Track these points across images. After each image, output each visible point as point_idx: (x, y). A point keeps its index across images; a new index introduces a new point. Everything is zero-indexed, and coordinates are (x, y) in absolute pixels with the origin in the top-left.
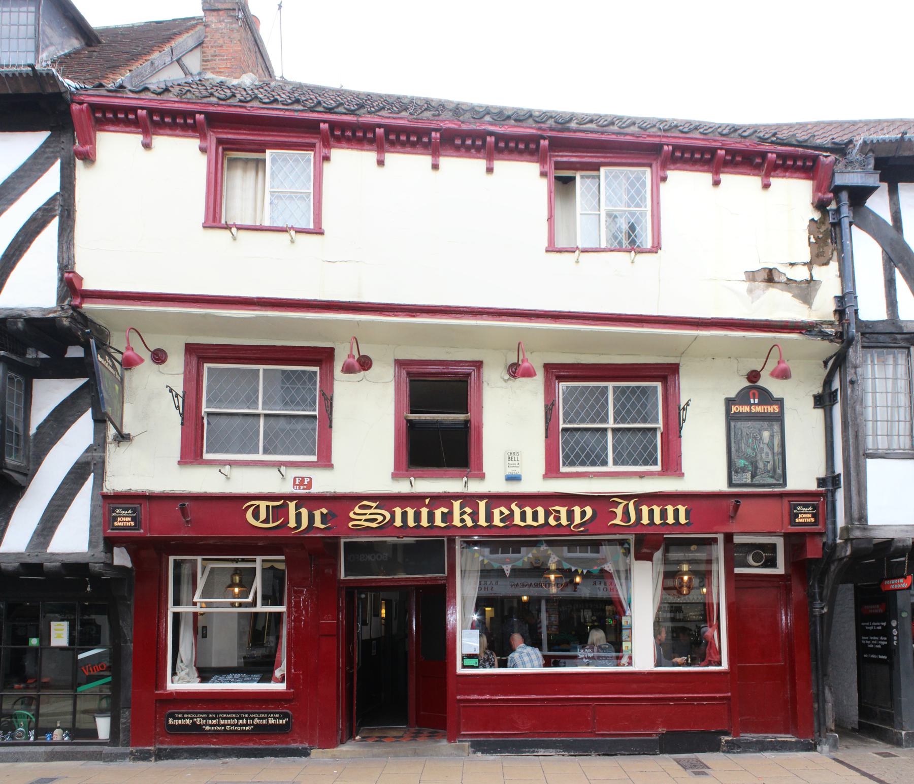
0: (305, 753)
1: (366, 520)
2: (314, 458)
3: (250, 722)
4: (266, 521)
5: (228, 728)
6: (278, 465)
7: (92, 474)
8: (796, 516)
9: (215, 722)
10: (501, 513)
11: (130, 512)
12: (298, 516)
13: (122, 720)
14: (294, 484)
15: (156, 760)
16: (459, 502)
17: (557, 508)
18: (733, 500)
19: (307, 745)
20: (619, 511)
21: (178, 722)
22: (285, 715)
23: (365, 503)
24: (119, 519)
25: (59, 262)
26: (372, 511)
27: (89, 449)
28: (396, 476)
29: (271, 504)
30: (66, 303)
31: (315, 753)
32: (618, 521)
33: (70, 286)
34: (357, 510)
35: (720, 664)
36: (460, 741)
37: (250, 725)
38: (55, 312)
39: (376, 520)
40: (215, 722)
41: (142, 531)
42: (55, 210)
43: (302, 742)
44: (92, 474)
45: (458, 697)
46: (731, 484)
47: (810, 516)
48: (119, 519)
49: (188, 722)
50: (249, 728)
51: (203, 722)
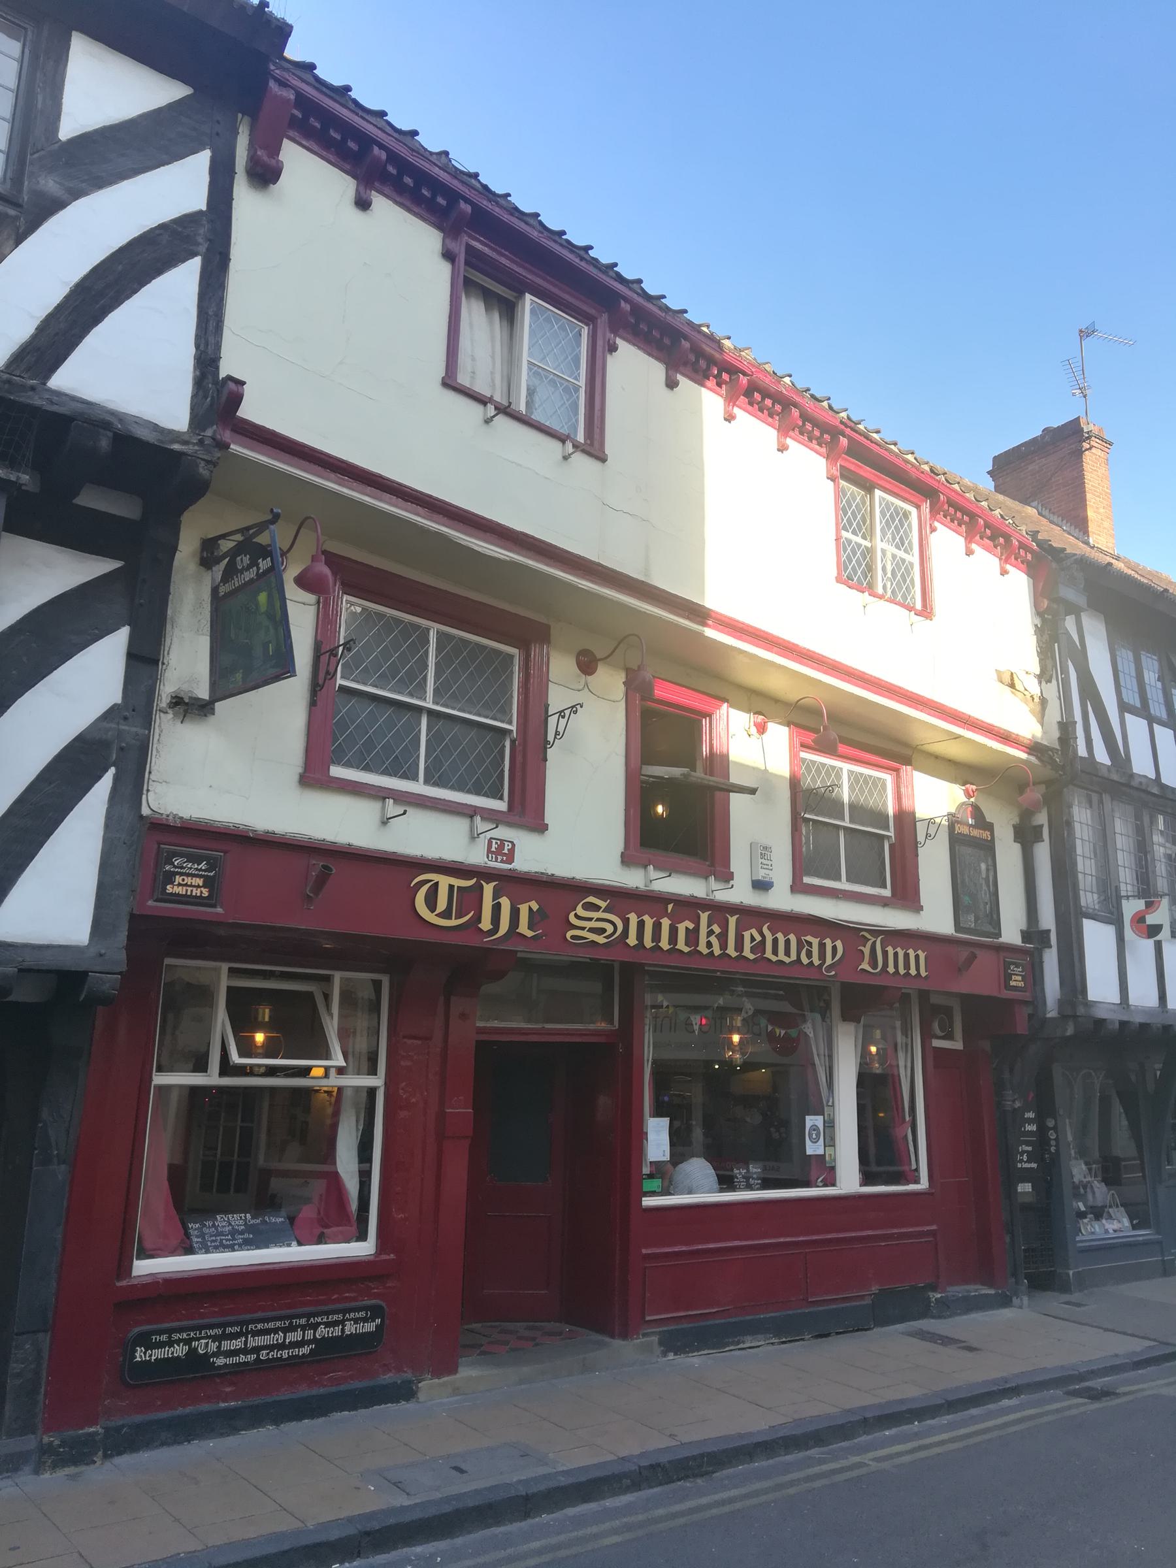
0: (406, 1392)
1: (591, 930)
2: (501, 806)
3: (309, 1334)
4: (446, 914)
5: (263, 1355)
6: (470, 813)
7: (112, 770)
8: (169, 878)
9: (238, 1344)
10: (753, 939)
11: (203, 866)
12: (497, 908)
13: (15, 1367)
14: (489, 851)
15: (106, 1456)
16: (707, 914)
17: (809, 938)
18: (318, 863)
19: (408, 1375)
20: (867, 950)
21: (157, 1354)
22: (376, 1312)
23: (591, 899)
24: (178, 879)
25: (197, 346)
26: (600, 915)
27: (111, 714)
28: (627, 860)
29: (458, 883)
30: (209, 432)
31: (427, 1386)
32: (865, 966)
33: (217, 397)
34: (579, 910)
35: (917, 1181)
36: (644, 1335)
37: (309, 1342)
38: (186, 443)
39: (604, 930)
40: (238, 1344)
41: (219, 910)
42: (198, 244)
43: (399, 1369)
44: (112, 770)
45: (644, 1251)
46: (958, 926)
47: (200, 882)
48: (178, 879)
49: (180, 1351)
50: (305, 1350)
51: (213, 1347)
